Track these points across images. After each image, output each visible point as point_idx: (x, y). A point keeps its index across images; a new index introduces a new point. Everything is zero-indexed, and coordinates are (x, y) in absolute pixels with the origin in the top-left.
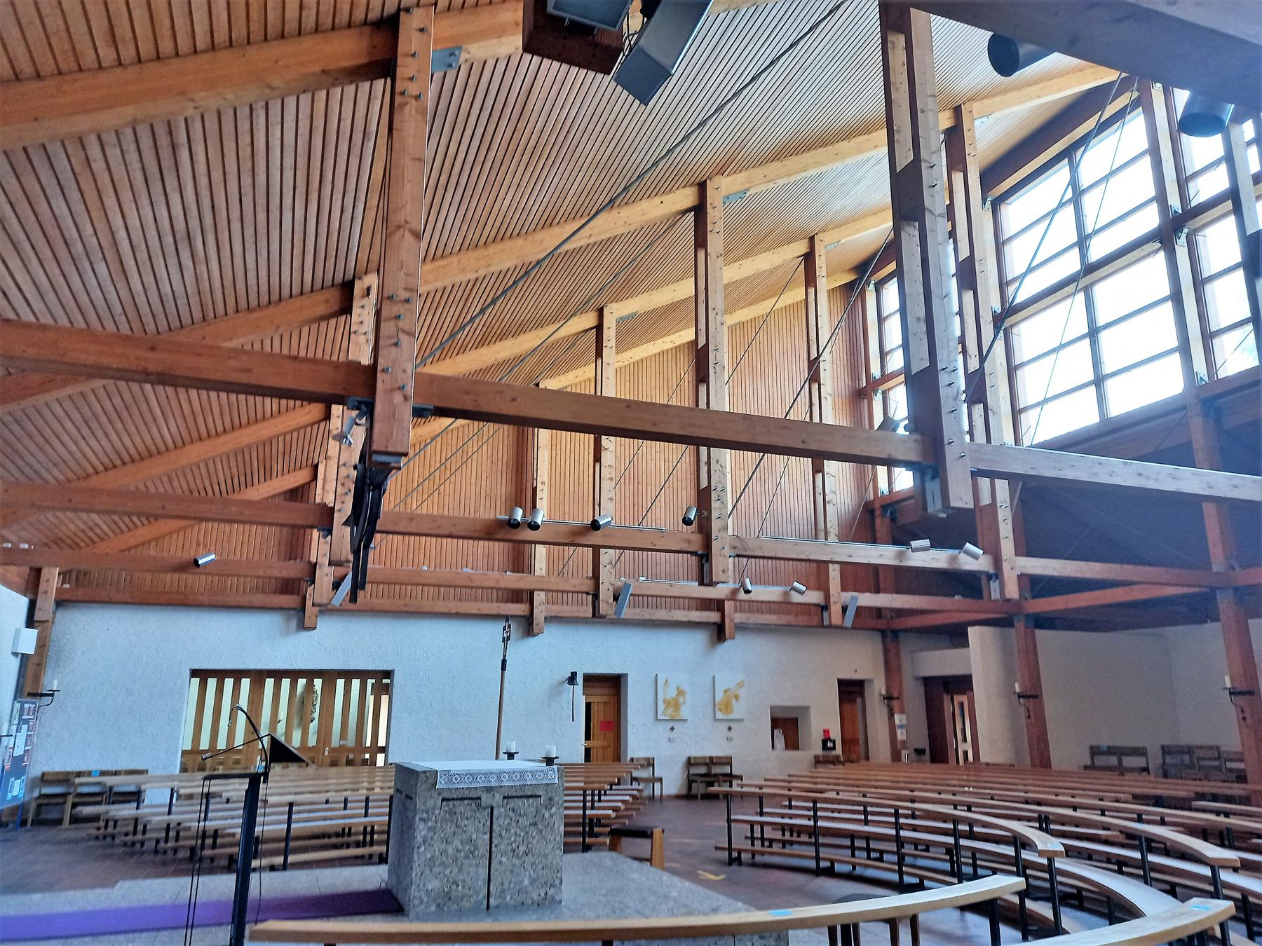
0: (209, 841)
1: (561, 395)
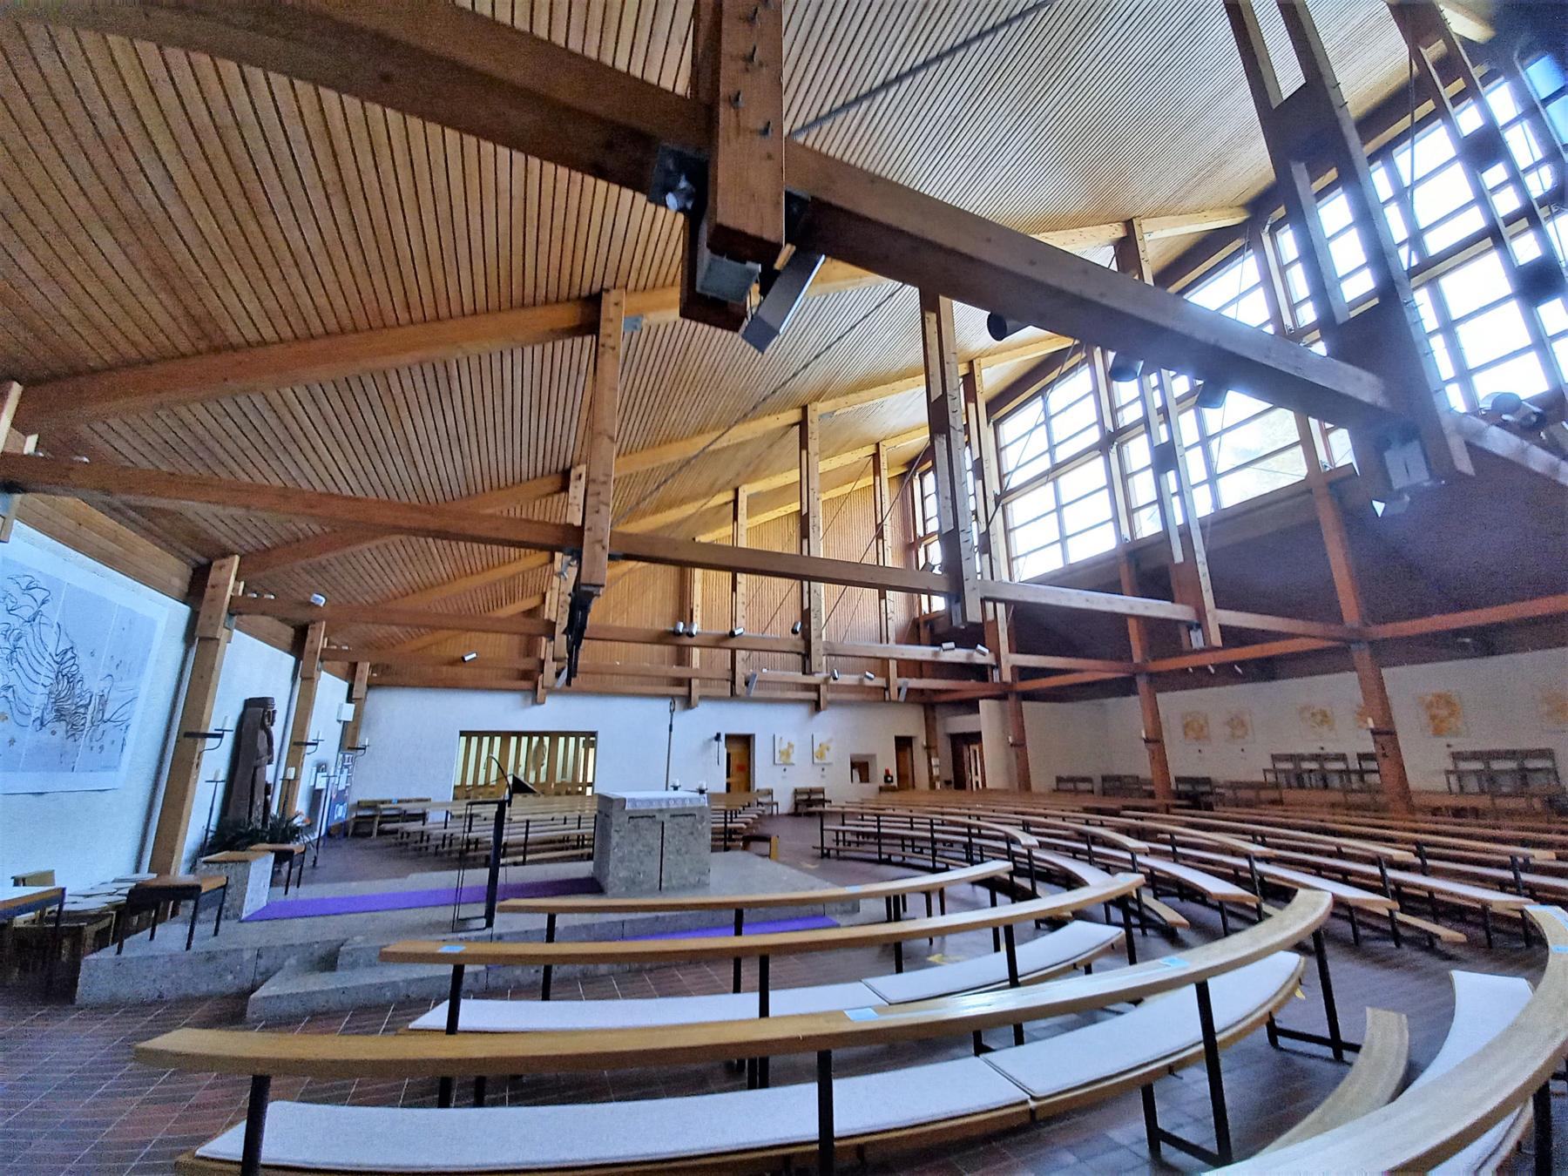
0: (472, 847)
1: (710, 546)
